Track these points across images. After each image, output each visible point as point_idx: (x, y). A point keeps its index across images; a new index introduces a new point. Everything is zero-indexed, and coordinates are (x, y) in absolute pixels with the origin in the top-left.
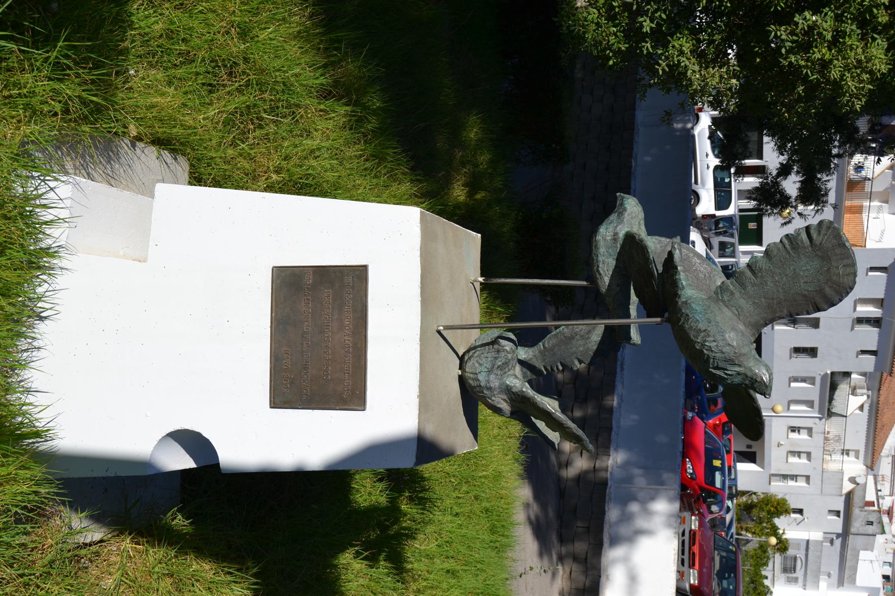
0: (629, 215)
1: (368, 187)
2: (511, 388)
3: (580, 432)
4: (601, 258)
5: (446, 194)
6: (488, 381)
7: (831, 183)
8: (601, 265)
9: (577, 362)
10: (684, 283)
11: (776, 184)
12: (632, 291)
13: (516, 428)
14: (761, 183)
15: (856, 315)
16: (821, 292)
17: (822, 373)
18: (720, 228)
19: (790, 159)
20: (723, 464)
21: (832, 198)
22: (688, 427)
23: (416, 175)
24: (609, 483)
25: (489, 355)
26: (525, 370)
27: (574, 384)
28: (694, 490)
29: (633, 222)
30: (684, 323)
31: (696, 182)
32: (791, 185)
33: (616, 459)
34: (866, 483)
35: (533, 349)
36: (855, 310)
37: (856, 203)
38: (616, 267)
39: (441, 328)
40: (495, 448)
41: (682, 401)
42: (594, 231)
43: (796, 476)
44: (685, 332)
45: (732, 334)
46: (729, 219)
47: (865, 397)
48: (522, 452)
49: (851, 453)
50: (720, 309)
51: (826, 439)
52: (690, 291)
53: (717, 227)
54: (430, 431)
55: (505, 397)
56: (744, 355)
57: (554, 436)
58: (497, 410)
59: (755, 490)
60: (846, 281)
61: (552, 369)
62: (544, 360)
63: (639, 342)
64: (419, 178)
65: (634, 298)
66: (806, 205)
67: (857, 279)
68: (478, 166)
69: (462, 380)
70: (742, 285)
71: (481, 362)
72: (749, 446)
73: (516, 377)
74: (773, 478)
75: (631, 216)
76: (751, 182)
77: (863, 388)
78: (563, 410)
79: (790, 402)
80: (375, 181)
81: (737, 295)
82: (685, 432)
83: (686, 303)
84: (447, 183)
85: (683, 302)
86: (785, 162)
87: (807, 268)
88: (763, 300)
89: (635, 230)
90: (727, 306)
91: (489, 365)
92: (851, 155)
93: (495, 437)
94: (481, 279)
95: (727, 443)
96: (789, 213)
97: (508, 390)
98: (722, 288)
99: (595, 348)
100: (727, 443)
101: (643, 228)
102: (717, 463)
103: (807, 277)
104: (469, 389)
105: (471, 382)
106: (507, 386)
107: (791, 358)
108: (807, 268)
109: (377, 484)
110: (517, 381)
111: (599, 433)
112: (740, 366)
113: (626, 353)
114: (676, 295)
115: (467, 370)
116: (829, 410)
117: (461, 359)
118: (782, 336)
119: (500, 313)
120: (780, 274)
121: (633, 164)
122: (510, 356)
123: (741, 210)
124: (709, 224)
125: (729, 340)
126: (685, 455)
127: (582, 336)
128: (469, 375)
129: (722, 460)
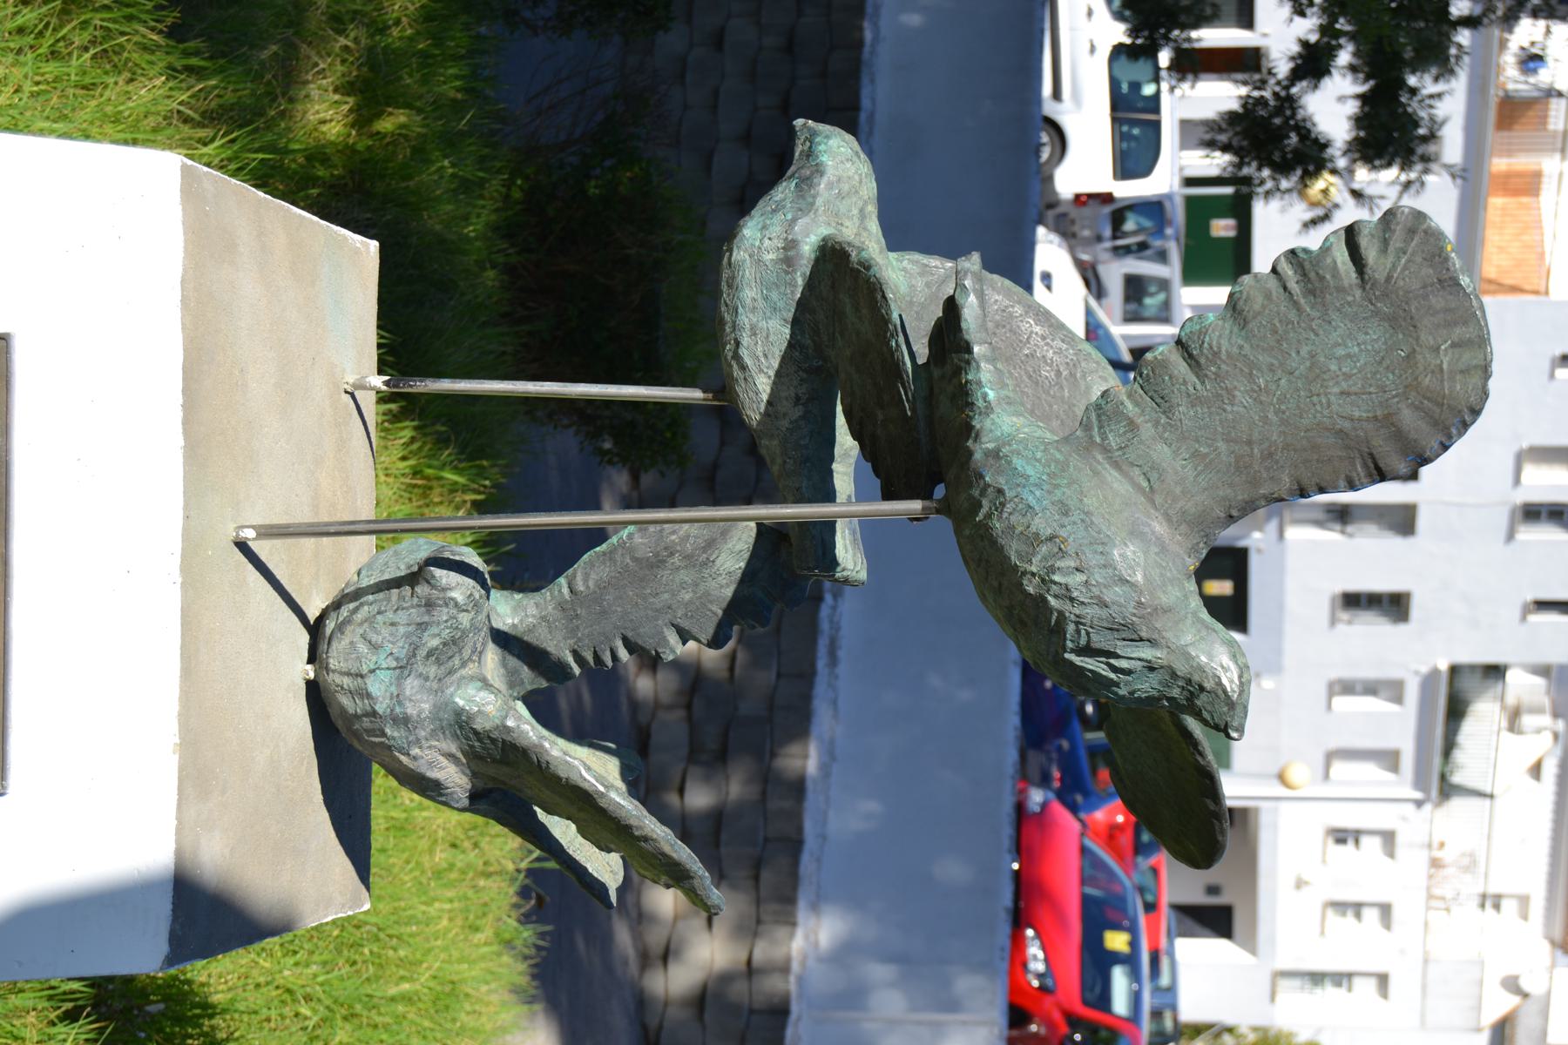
0: (830, 186)
1: (28, 87)
2: (471, 717)
3: (683, 853)
4: (745, 319)
5: (282, 114)
6: (398, 698)
7: (1447, 102)
8: (746, 340)
9: (673, 638)
10: (991, 395)
11: (1287, 103)
12: (840, 420)
13: (504, 848)
14: (1246, 101)
15: (1523, 496)
16: (1388, 421)
17: (1424, 669)
18: (1125, 235)
19: (1326, 30)
20: (1134, 944)
21: (1452, 145)
22: (1027, 830)
23: (187, 54)
24: (795, 1008)
25: (402, 617)
26: (513, 662)
27: (689, 707)
28: (1050, 1024)
29: (843, 207)
30: (989, 516)
31: (1057, 94)
32: (1332, 108)
33: (812, 937)
34: (1549, 993)
35: (537, 597)
36: (1517, 481)
37: (1522, 162)
38: (791, 345)
39: (249, 534)
40: (441, 909)
41: (1012, 755)
42: (729, 235)
43: (1350, 976)
44: (993, 542)
45: (1131, 550)
46: (1153, 208)
47: (1547, 737)
48: (525, 919)
49: (1505, 903)
50: (1096, 473)
51: (1436, 864)
52: (1006, 419)
53: (1117, 231)
54: (218, 858)
55: (453, 748)
56: (1167, 610)
57: (606, 867)
58: (429, 788)
59: (1228, 1019)
60: (1460, 389)
61: (597, 657)
62: (572, 632)
63: (863, 575)
64: (194, 61)
65: (845, 441)
66: (1374, 168)
67: (1492, 384)
68: (383, 30)
69: (315, 692)
70: (1161, 401)
71: (374, 638)
72: (1213, 890)
73: (486, 684)
74: (1283, 984)
75: (836, 190)
76: (1218, 96)
77: (1538, 710)
78: (641, 785)
79: (1331, 756)
80: (51, 68)
81: (1147, 431)
82: (1019, 848)
83: (995, 454)
84: (286, 80)
85: (988, 453)
86: (1313, 38)
87: (1350, 349)
88: (1221, 445)
89: (848, 233)
90: (1116, 465)
91: (400, 649)
92: (1510, 19)
93: (438, 874)
94: (378, 381)
95: (1148, 880)
96: (1325, 192)
97: (461, 725)
98: (1104, 410)
99: (729, 592)
100: (1148, 880)
101: (874, 226)
102: (1117, 941)
103: (1348, 376)
104: (339, 724)
105: (345, 701)
106: (459, 712)
107: (1333, 621)
108: (1350, 349)
109: (61, 1029)
110: (490, 696)
111: (760, 854)
112: (1152, 643)
113: (843, 619)
114: (967, 430)
115: (333, 663)
116: (1443, 777)
117: (315, 629)
118: (1303, 561)
119: (454, 489)
120: (1271, 369)
121: (868, 35)
122: (465, 619)
123: (1190, 182)
124: (1105, 223)
125: (1121, 566)
126: (1019, 920)
127: (687, 557)
128: (338, 679)
129: (1133, 930)
